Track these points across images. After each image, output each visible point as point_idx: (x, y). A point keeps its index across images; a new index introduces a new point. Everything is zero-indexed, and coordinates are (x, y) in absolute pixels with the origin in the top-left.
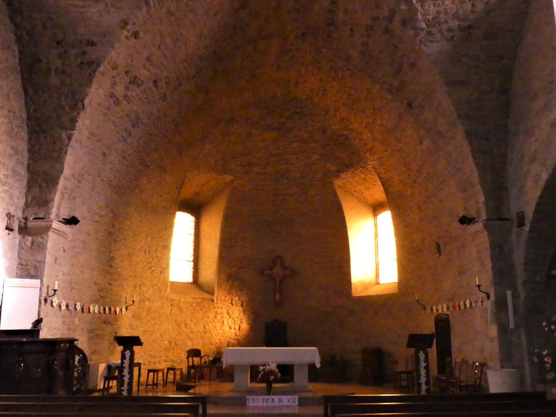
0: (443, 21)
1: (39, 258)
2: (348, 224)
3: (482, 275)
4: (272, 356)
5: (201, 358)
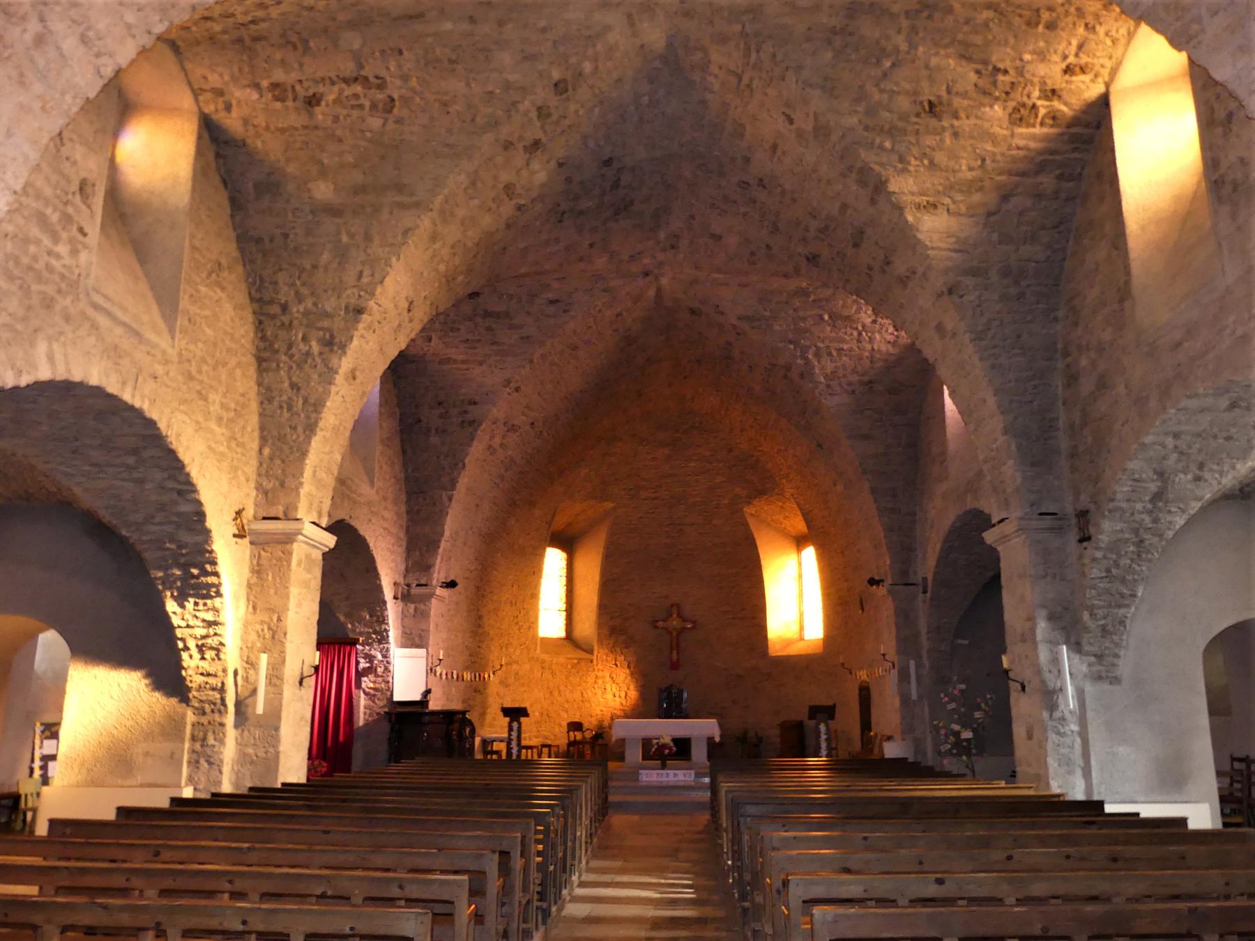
1: (423, 626)
2: (764, 563)
3: (888, 645)
4: (666, 729)
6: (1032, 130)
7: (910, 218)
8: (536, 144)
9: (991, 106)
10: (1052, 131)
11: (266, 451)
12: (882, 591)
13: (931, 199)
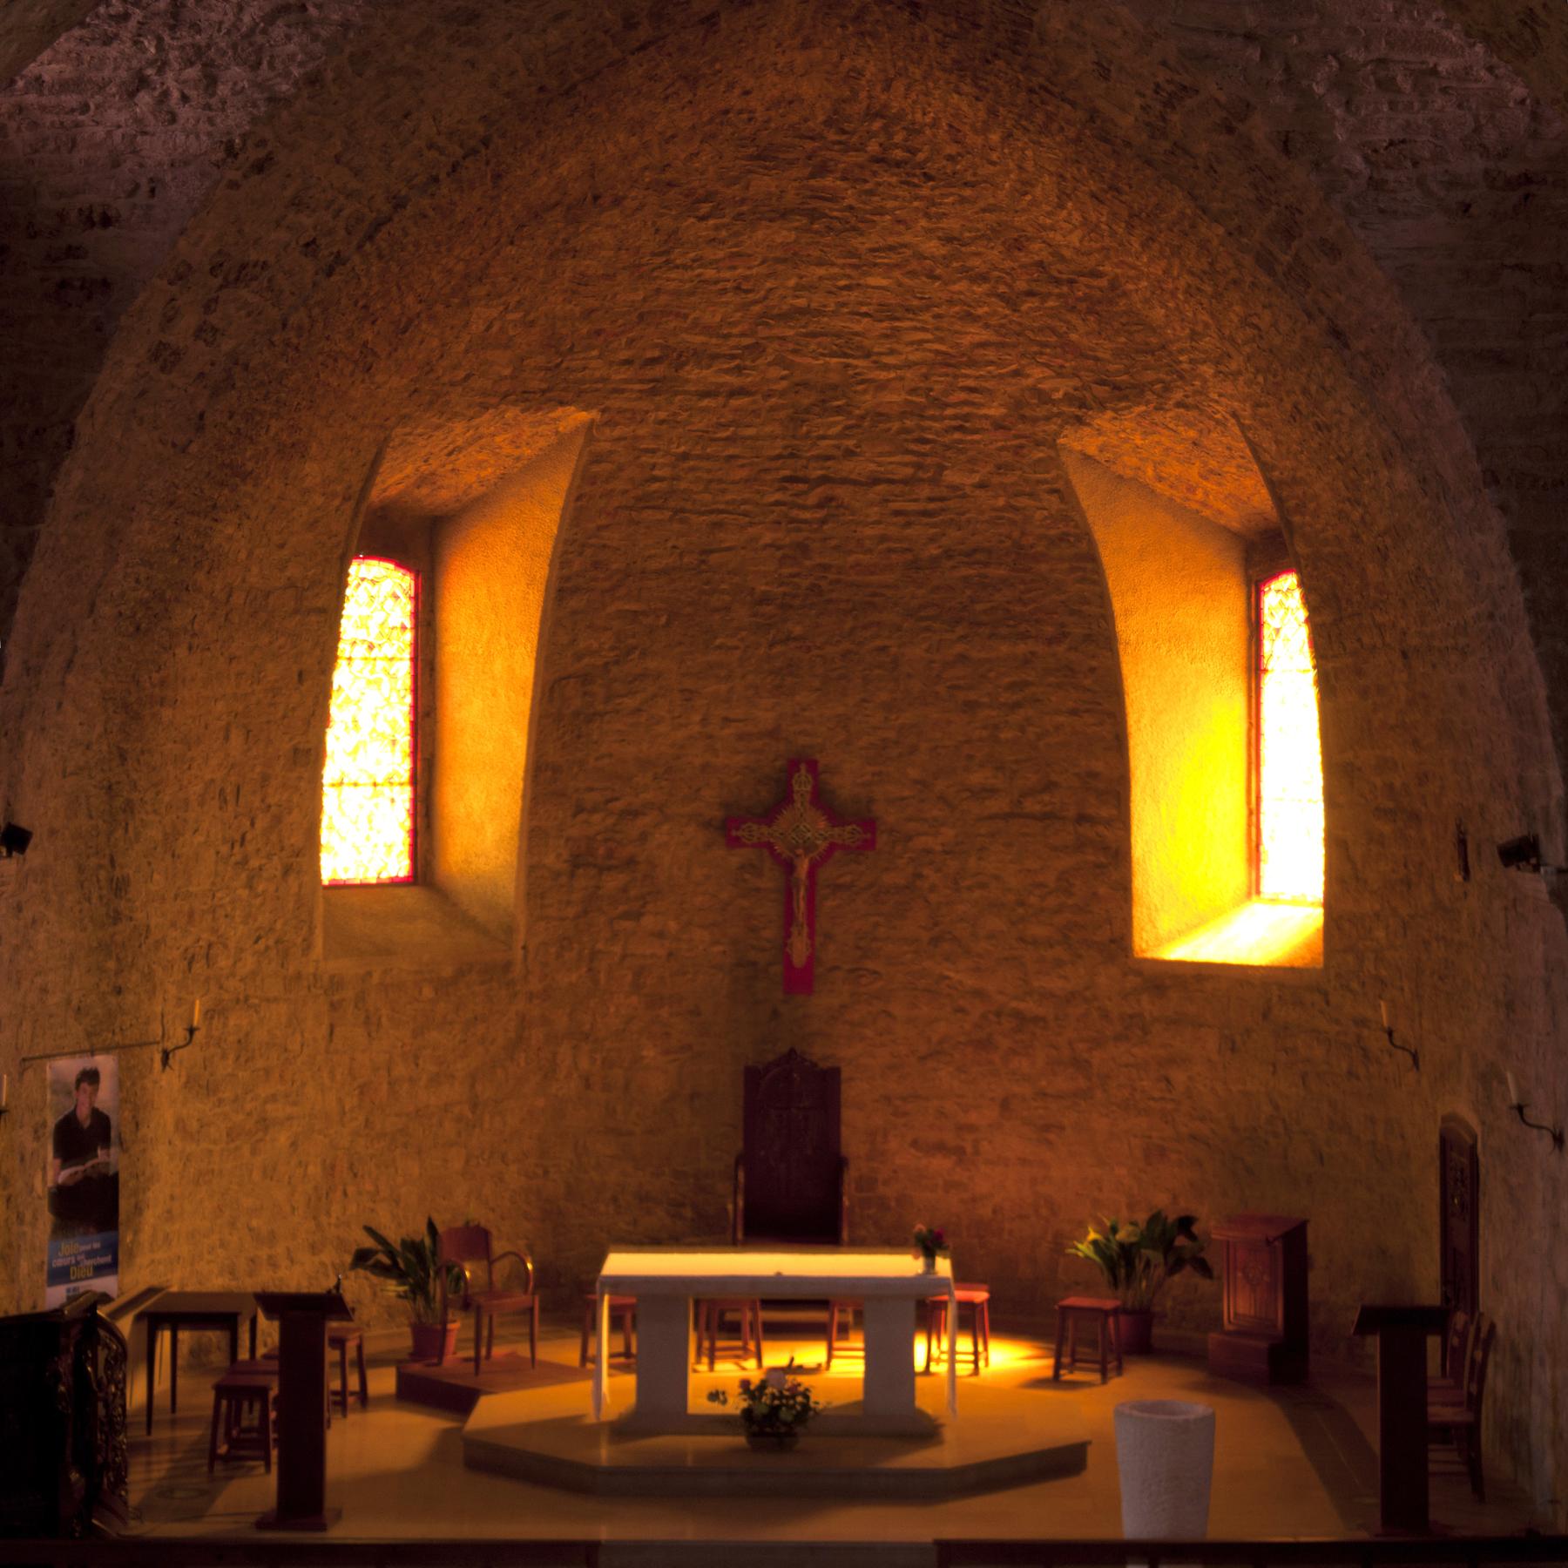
0: (1427, 155)
5: (491, 1263)
12: (1535, 885)
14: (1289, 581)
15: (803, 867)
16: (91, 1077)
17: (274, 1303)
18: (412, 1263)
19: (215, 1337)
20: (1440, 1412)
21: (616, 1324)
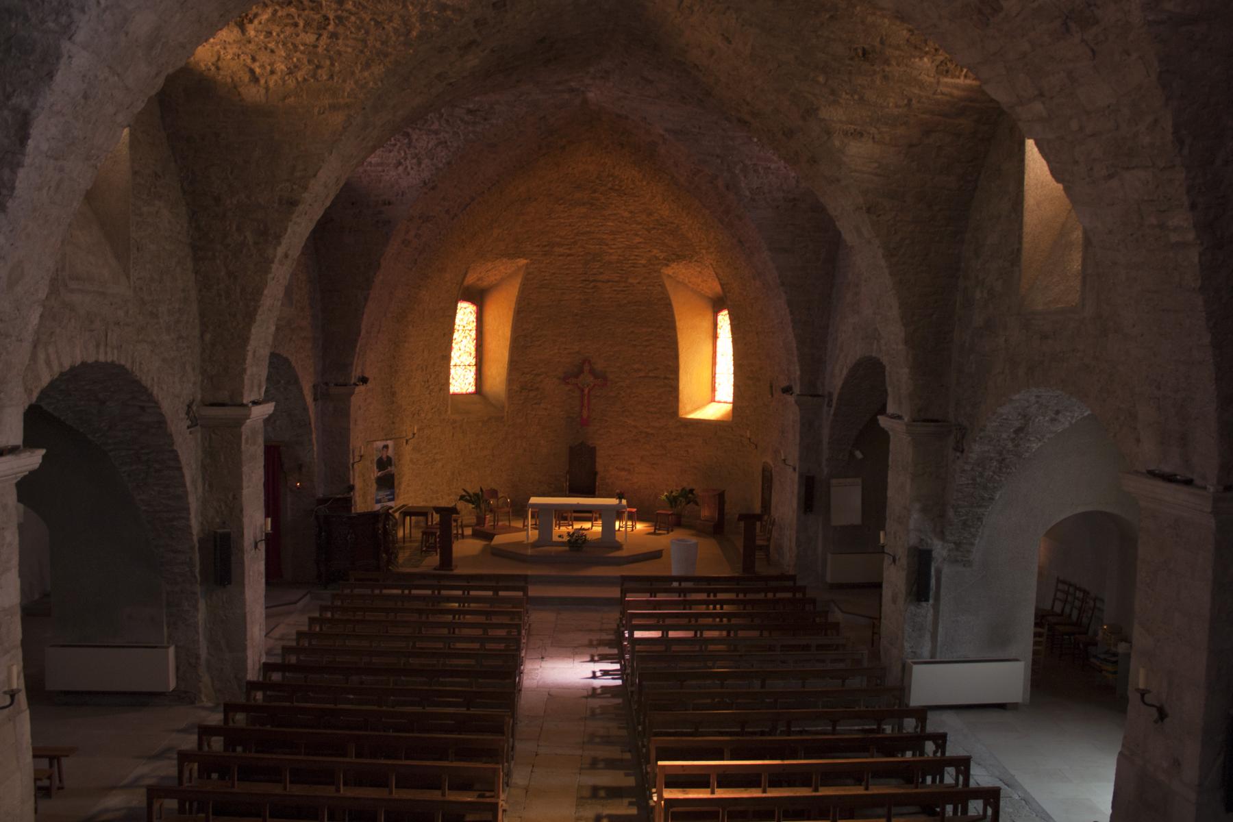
6: (957, 81)
7: (837, 143)
8: (473, 43)
9: (921, 58)
10: (975, 83)
11: (208, 337)
12: (791, 399)
13: (859, 128)
14: (726, 312)
15: (586, 391)
16: (386, 447)
17: (438, 510)
18: (476, 499)
19: (421, 518)
20: (759, 542)
21: (533, 517)
